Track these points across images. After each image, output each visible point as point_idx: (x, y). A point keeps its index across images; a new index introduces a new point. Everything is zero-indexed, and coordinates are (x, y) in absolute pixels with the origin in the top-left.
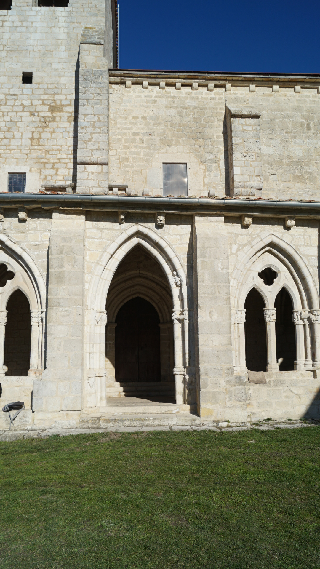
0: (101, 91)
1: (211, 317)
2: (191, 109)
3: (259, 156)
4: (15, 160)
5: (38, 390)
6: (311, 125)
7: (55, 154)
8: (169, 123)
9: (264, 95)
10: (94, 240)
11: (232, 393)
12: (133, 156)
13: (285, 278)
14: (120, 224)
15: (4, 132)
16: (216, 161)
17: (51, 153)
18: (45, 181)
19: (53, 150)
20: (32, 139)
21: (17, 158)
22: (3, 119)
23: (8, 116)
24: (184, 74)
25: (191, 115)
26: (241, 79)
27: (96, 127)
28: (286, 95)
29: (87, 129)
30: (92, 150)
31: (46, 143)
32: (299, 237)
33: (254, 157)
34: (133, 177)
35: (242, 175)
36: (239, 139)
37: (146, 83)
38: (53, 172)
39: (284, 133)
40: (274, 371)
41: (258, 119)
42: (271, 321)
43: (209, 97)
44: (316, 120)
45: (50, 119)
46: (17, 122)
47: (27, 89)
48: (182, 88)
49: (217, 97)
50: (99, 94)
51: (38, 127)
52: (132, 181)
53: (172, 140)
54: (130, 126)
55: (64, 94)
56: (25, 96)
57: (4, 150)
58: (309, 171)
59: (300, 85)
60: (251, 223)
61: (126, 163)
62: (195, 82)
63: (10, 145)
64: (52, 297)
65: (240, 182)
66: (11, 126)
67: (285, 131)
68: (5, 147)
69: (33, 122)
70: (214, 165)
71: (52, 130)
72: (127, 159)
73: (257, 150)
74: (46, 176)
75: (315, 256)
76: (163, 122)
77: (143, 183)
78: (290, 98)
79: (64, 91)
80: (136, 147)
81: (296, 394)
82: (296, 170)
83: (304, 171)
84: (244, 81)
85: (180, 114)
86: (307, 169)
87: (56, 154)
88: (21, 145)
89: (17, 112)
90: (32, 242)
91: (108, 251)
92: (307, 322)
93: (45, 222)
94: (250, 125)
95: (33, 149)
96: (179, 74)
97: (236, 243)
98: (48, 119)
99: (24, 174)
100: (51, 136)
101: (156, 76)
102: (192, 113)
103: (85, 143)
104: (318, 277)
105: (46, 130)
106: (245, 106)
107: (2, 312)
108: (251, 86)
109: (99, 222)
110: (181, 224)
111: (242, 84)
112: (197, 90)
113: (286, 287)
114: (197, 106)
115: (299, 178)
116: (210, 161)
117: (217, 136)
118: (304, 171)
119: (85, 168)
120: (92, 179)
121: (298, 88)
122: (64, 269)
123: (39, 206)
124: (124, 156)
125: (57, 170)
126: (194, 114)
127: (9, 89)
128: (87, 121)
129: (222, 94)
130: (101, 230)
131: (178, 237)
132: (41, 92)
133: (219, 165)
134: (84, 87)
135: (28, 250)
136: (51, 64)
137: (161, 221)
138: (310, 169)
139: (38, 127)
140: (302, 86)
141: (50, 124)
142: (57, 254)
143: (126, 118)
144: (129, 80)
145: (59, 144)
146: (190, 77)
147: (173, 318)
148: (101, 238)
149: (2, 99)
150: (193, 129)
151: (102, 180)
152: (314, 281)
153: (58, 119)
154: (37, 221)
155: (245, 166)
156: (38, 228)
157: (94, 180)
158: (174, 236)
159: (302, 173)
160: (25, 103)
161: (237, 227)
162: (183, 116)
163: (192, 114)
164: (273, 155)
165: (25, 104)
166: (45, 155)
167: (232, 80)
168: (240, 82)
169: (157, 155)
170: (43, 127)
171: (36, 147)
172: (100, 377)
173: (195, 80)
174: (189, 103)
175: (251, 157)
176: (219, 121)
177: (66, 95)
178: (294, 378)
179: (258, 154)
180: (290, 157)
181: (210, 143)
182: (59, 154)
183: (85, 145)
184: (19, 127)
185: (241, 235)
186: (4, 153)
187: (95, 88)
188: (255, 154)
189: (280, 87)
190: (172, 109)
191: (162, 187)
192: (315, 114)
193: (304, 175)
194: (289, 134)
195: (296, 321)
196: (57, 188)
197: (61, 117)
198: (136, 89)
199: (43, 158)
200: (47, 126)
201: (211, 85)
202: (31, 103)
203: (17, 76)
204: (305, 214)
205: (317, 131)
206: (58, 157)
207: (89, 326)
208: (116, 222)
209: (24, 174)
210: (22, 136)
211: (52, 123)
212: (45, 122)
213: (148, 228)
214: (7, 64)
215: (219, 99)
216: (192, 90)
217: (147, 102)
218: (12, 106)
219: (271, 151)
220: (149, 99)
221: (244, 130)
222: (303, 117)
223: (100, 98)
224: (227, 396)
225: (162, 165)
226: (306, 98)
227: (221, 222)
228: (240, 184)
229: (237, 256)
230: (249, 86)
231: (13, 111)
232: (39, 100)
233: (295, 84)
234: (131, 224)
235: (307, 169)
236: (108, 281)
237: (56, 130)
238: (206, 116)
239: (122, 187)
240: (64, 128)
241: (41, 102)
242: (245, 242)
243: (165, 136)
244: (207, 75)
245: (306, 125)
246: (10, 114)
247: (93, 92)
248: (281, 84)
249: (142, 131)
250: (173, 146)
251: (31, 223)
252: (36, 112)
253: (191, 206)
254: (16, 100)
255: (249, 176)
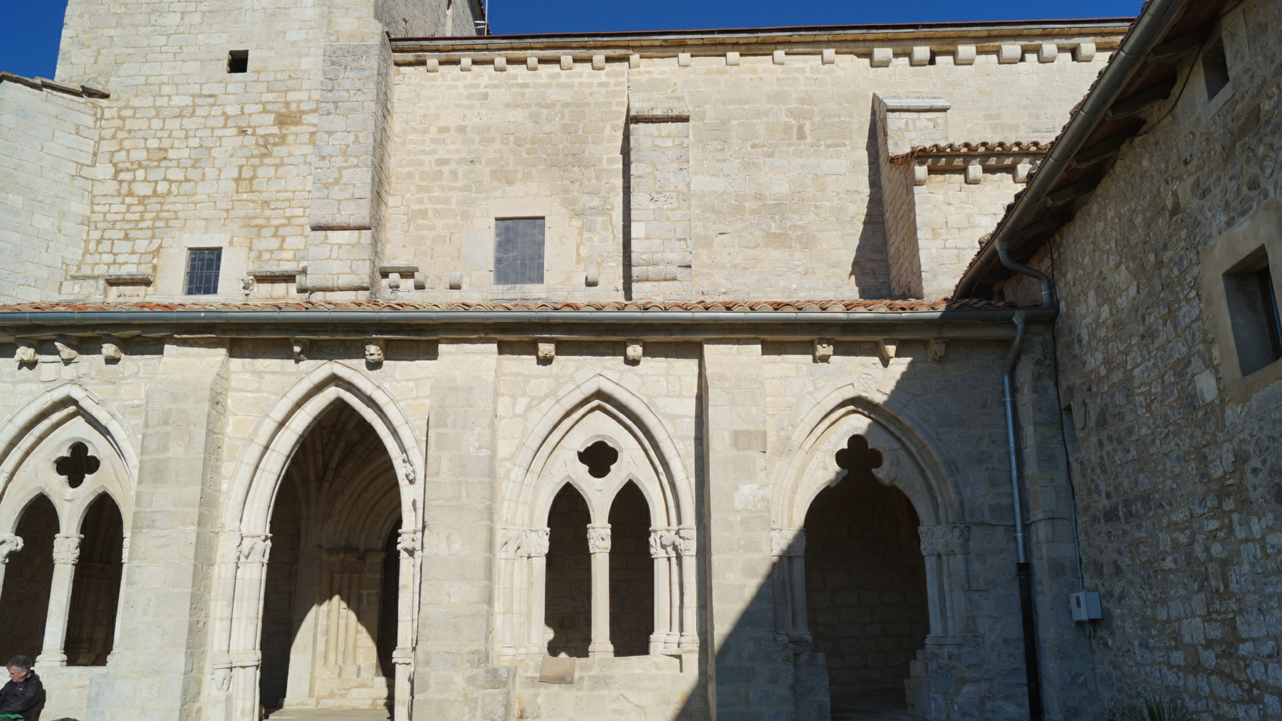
0: (364, 86)
1: (449, 546)
2: (558, 108)
3: (685, 198)
4: (204, 223)
5: (97, 695)
6: (807, 128)
7: (281, 209)
8: (512, 138)
9: (710, 72)
10: (246, 394)
11: (477, 702)
12: (436, 206)
13: (632, 463)
14: (297, 361)
15: (186, 168)
16: (604, 211)
17: (272, 207)
18: (257, 263)
19: (278, 200)
20: (238, 180)
21: (206, 219)
22: (185, 144)
23: (195, 137)
24: (540, 40)
25: (557, 119)
26: (658, 43)
27: (350, 155)
28: (754, 71)
29: (332, 159)
30: (339, 201)
31: (264, 188)
32: (656, 378)
33: (674, 201)
34: (433, 249)
35: (647, 238)
36: (644, 166)
37: (466, 61)
38: (275, 243)
39: (749, 148)
40: (598, 656)
41: (685, 124)
42: (597, 551)
43: (596, 81)
44: (818, 118)
45: (277, 140)
46: (212, 148)
47: (236, 83)
48: (541, 66)
49: (612, 81)
50: (358, 90)
51: (253, 156)
52: (432, 258)
53: (517, 171)
54: (433, 147)
55: (306, 90)
56: (230, 97)
57: (183, 204)
58: (800, 223)
59: (783, 49)
60: (553, 353)
61: (420, 222)
62: (564, 54)
63: (194, 195)
64: (142, 509)
65: (645, 253)
66: (199, 157)
67: (750, 143)
68: (185, 199)
69: (243, 146)
70: (600, 219)
71: (277, 161)
72: (423, 214)
73: (682, 187)
74: (260, 253)
75: (690, 417)
76: (499, 135)
77: (453, 260)
78: (763, 76)
79: (306, 85)
80: (442, 188)
81: (637, 706)
82: (772, 223)
83: (789, 223)
84: (666, 46)
85: (535, 118)
86: (796, 219)
87: (284, 209)
88: (217, 193)
89: (213, 129)
90: (127, 400)
91: (272, 414)
92: (673, 554)
93: (155, 361)
94: (669, 136)
95: (238, 201)
96: (530, 40)
97: (524, 395)
98: (271, 140)
99: (219, 250)
100: (276, 172)
101: (485, 47)
102: (559, 116)
103: (327, 188)
104: (693, 460)
105: (266, 161)
106: (666, 98)
107: (67, 538)
108: (680, 55)
109: (256, 360)
110: (418, 359)
111: (662, 52)
112: (571, 69)
113: (635, 481)
114: (570, 100)
115: (777, 239)
116: (593, 211)
117: (608, 159)
118: (789, 223)
119: (326, 237)
120: (338, 258)
121: (779, 54)
122: (169, 454)
123: (137, 332)
124: (417, 207)
125: (283, 241)
126: (562, 118)
127: (202, 85)
128: (333, 145)
129: (623, 75)
130: (259, 374)
131: (411, 384)
132: (263, 87)
133: (611, 218)
134: (330, 79)
135: (121, 417)
136: (285, 33)
137: (371, 355)
138: (801, 219)
139: (253, 156)
140: (787, 50)
141: (276, 149)
142: (158, 425)
143: (426, 131)
144: (433, 57)
145: (290, 187)
146: (553, 44)
147: (399, 547)
148: (258, 390)
149: (187, 106)
150: (560, 146)
151: (357, 260)
152: (685, 468)
153: (290, 139)
154: (140, 361)
155: (655, 220)
156: (141, 374)
157: (342, 260)
158: (403, 383)
159: (785, 228)
160: (232, 110)
161: (527, 362)
162: (541, 122)
163: (560, 118)
164: (723, 193)
165: (229, 113)
166: (263, 210)
167: (642, 47)
168: (658, 49)
169: (484, 203)
170: (263, 156)
171: (245, 196)
172: (243, 667)
173: (565, 51)
174: (553, 95)
175: (669, 200)
176: (614, 128)
177: (309, 91)
178: (639, 671)
179: (684, 194)
180: (759, 197)
181: (593, 175)
182: (290, 207)
183: (326, 191)
184: (215, 158)
185: (537, 377)
186: (183, 210)
187: (353, 79)
188: (678, 196)
189: (741, 55)
190: (519, 109)
191: (492, 267)
192: (816, 105)
193: (790, 232)
194: (760, 150)
195: (652, 551)
196: (278, 276)
197: (297, 135)
198: (449, 73)
199: (258, 218)
200: (268, 155)
201: (599, 57)
202: (242, 109)
203: (219, 60)
204: (658, 334)
205: (819, 141)
206: (287, 215)
207: (223, 566)
208: (289, 358)
209: (219, 250)
210: (219, 175)
211: (279, 148)
212: (266, 147)
213: (349, 369)
214: (201, 37)
215: (615, 85)
216: (561, 69)
217: (470, 97)
218: (205, 117)
219: (720, 185)
220: (473, 91)
221: (656, 148)
222: (791, 113)
223: (362, 98)
224: (466, 709)
225: (493, 222)
226: (797, 75)
227: (492, 353)
228: (643, 257)
229: (526, 420)
230: (677, 56)
231: (205, 127)
232: (256, 104)
233: (773, 47)
234: (320, 362)
235: (796, 219)
236: (273, 474)
237: (286, 160)
238: (587, 121)
239: (406, 270)
240: (302, 155)
241: (260, 107)
242: (545, 391)
243: (503, 163)
244: (586, 39)
245: (795, 130)
246: (199, 133)
247: (348, 86)
248: (743, 48)
249: (456, 157)
250: (518, 184)
251: (128, 363)
252: (250, 127)
253: (426, 325)
254: (214, 105)
255: (663, 240)
